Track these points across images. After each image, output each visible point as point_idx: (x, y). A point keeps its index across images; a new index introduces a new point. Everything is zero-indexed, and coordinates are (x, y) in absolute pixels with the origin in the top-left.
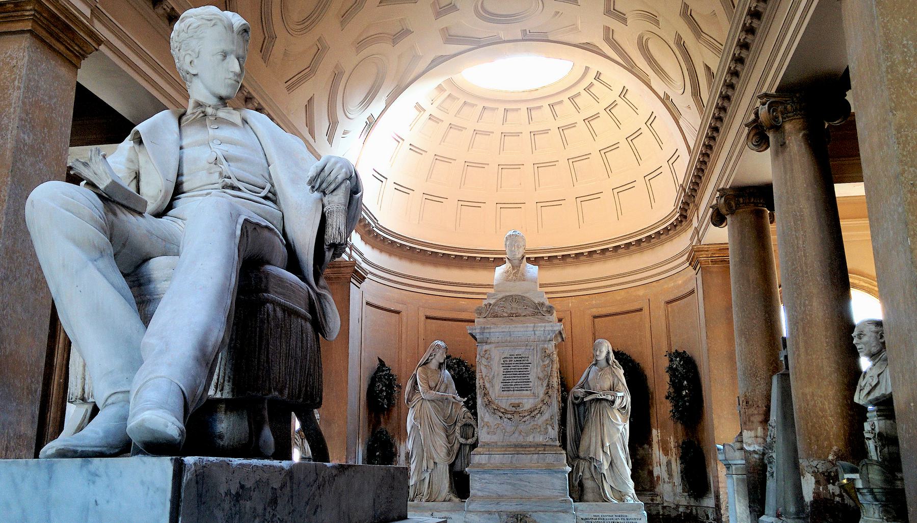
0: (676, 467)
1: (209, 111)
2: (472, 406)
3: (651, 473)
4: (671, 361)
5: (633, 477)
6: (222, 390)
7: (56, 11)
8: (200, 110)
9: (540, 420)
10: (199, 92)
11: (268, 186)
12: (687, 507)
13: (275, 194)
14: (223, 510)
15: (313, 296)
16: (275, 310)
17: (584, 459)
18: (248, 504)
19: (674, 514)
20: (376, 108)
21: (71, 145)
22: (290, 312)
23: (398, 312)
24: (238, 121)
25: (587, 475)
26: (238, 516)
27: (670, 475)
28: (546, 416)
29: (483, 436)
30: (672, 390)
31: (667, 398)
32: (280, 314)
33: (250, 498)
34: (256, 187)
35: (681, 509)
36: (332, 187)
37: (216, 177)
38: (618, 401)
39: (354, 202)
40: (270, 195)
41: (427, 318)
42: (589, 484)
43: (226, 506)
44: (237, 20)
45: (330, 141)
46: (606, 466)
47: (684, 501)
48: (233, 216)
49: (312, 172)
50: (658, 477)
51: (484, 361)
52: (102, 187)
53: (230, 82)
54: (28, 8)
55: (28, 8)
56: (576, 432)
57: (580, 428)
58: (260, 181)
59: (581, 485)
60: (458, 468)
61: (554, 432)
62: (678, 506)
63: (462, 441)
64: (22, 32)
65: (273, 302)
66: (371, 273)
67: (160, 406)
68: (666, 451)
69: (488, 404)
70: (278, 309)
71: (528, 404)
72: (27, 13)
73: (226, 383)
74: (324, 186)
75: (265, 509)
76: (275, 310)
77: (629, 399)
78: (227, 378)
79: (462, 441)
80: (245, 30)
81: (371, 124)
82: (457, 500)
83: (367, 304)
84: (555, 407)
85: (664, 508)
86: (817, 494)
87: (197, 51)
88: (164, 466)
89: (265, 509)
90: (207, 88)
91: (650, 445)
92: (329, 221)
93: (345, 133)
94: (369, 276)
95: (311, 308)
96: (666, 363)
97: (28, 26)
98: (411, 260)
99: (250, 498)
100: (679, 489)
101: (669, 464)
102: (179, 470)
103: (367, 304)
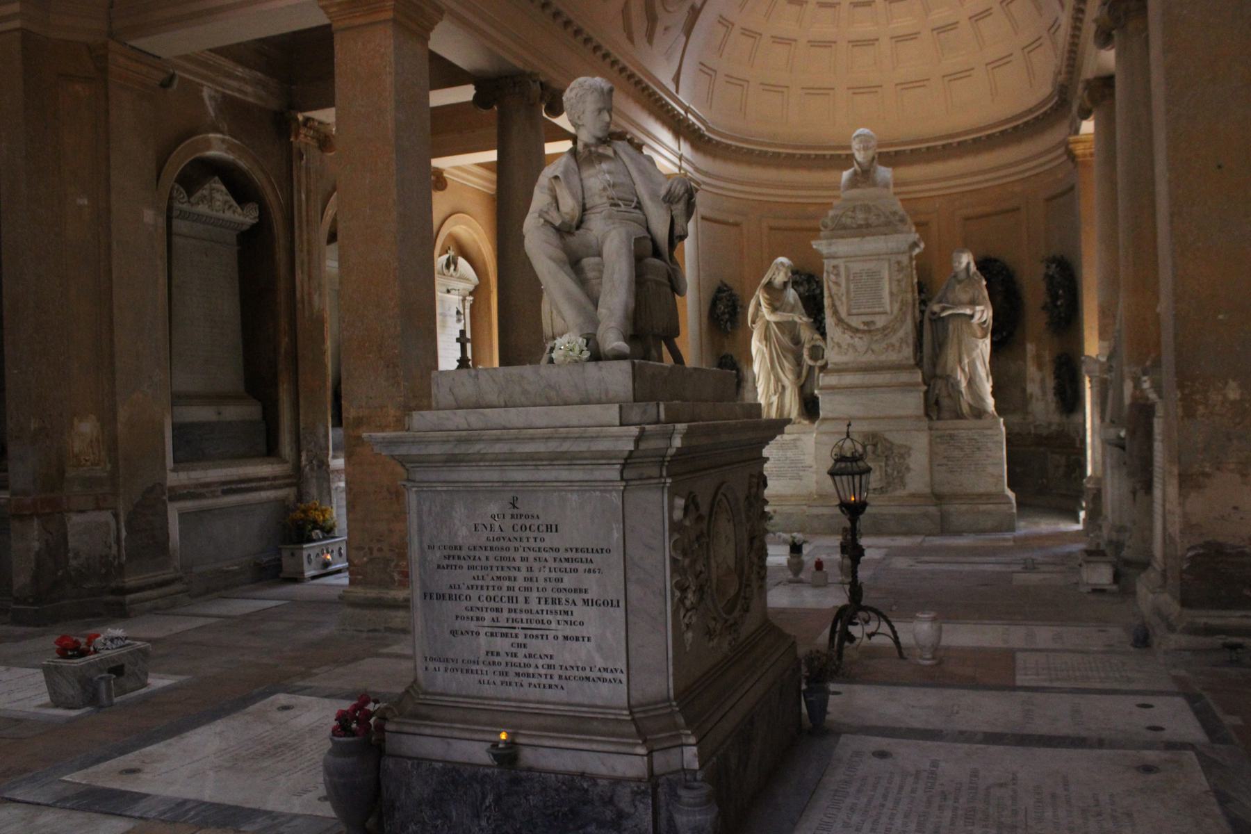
0: (1051, 383)
1: (593, 149)
2: (820, 328)
3: (1024, 390)
4: (1048, 267)
5: (994, 394)
9: (894, 340)
12: (1059, 425)
17: (941, 377)
19: (1045, 432)
21: (329, 26)
22: (658, 283)
25: (944, 393)
27: (1044, 393)
28: (901, 333)
29: (832, 356)
30: (1048, 300)
31: (1043, 308)
34: (628, 202)
35: (1054, 427)
37: (605, 200)
38: (977, 316)
41: (771, 228)
42: (945, 402)
46: (963, 384)
47: (1056, 418)
48: (628, 233)
50: (1031, 395)
51: (833, 277)
56: (934, 349)
57: (940, 346)
58: (631, 197)
59: (937, 403)
60: (808, 391)
61: (908, 352)
62: (1050, 424)
63: (811, 363)
64: (385, 21)
66: (704, 183)
67: (618, 340)
68: (1040, 366)
69: (840, 321)
71: (881, 322)
77: (991, 314)
79: (811, 363)
82: (806, 422)
84: (908, 327)
85: (1036, 427)
86: (1133, 397)
88: (625, 365)
91: (1025, 362)
93: (666, 29)
94: (703, 187)
95: (670, 280)
96: (1041, 270)
97: (390, 15)
98: (749, 163)
100: (1053, 406)
101: (1043, 381)
102: (633, 365)
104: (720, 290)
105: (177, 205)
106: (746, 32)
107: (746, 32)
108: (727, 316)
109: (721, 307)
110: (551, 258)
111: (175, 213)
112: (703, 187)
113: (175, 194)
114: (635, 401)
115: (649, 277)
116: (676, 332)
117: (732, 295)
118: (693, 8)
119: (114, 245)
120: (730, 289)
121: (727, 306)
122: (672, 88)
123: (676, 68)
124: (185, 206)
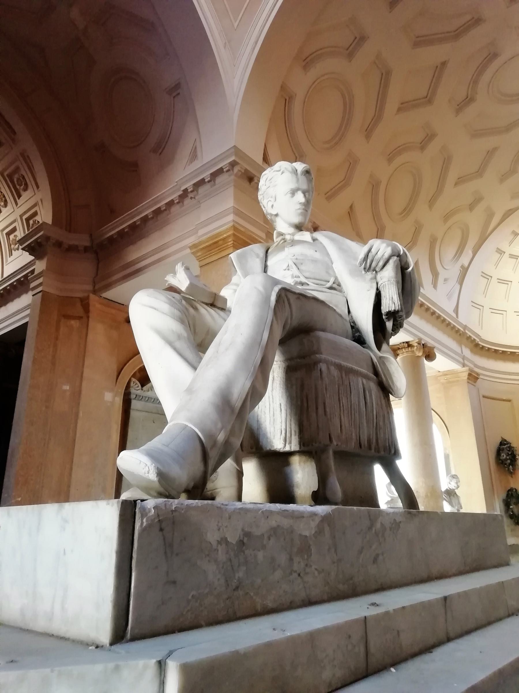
1: (288, 237)
6: (290, 443)
7: (244, 238)
8: (281, 237)
10: (282, 226)
11: (332, 280)
13: (339, 285)
14: (216, 561)
15: (375, 360)
16: (328, 368)
18: (260, 555)
20: (465, 260)
23: (509, 401)
24: (309, 239)
26: (244, 568)
32: (335, 372)
33: (264, 547)
36: (381, 264)
39: (407, 278)
40: (335, 286)
43: (221, 556)
44: (300, 166)
45: (435, 286)
49: (362, 256)
52: (183, 289)
53: (300, 211)
54: (230, 240)
55: (230, 240)
65: (327, 362)
70: (332, 368)
72: (229, 243)
73: (293, 437)
74: (374, 265)
75: (291, 559)
76: (328, 368)
78: (293, 433)
80: (307, 172)
81: (464, 271)
83: (484, 397)
87: (274, 196)
89: (291, 559)
90: (285, 221)
92: (383, 294)
93: (446, 280)
99: (264, 547)
103: (484, 397)
104: (501, 444)
105: (132, 390)
106: (501, 281)
107: (501, 281)
108: (509, 461)
109: (504, 456)
110: (159, 333)
111: (133, 396)
112: (481, 377)
113: (132, 384)
114: (119, 635)
115: (323, 356)
116: (395, 453)
117: (510, 447)
118: (462, 267)
119: (81, 414)
120: (508, 443)
121: (508, 455)
122: (454, 315)
123: (455, 304)
124: (139, 392)
